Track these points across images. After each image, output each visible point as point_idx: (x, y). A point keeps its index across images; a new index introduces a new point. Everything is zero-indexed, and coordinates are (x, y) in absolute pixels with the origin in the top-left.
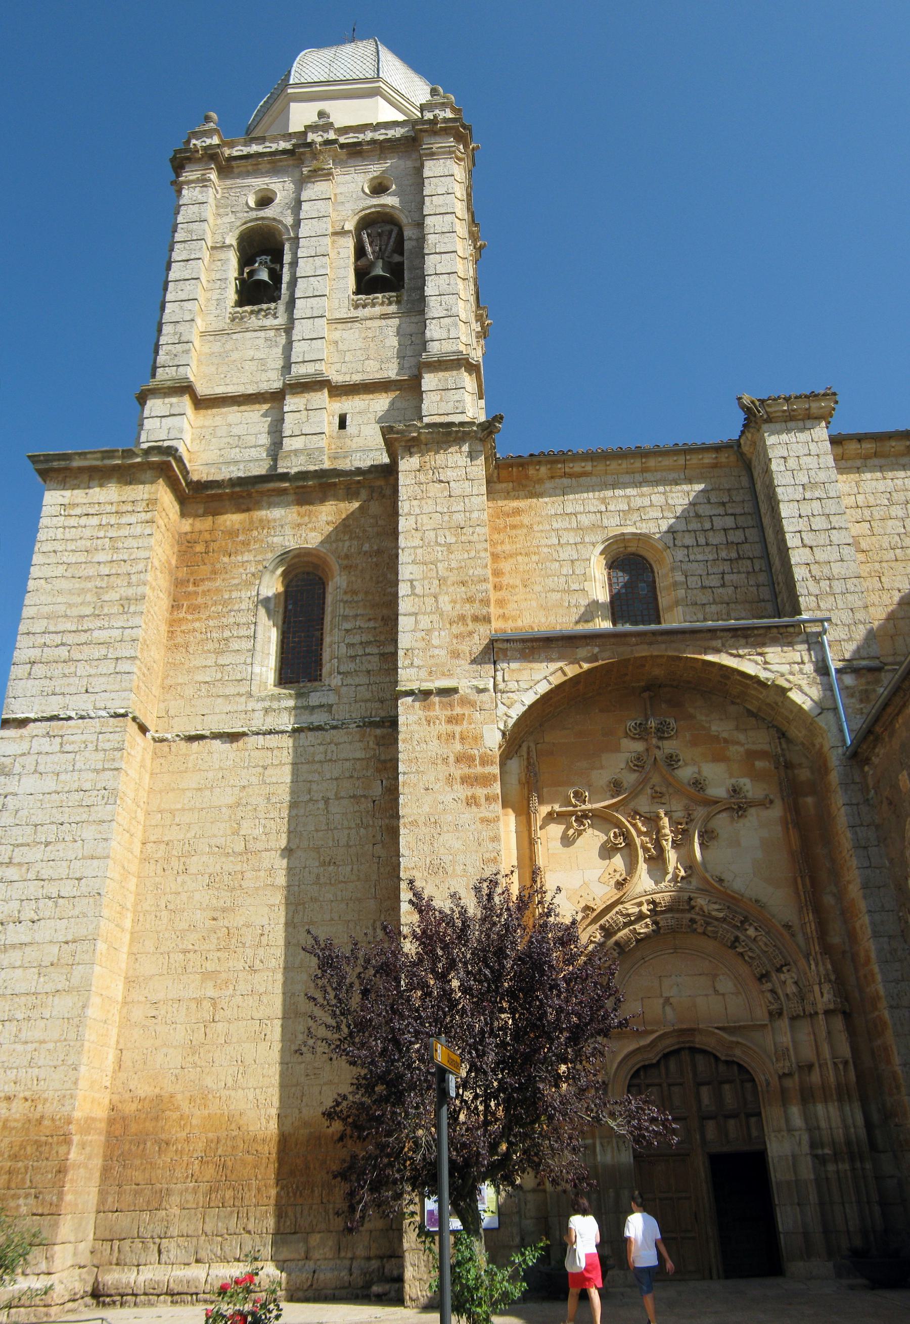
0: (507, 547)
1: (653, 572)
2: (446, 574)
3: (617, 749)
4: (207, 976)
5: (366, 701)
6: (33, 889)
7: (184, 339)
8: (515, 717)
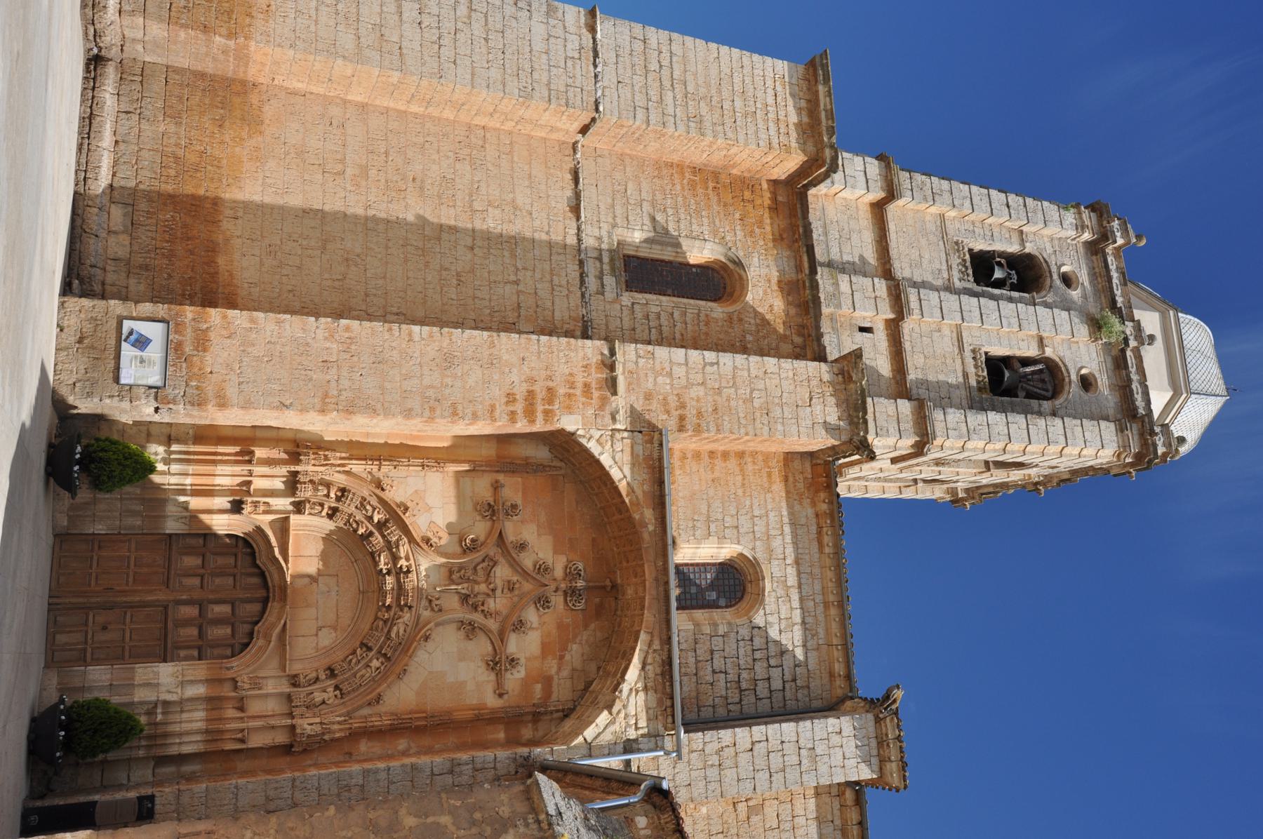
0: (750, 467)
1: (727, 607)
2: (724, 395)
3: (556, 552)
4: (364, 170)
5: (607, 325)
6: (448, 25)
7: (937, 197)
8: (589, 446)
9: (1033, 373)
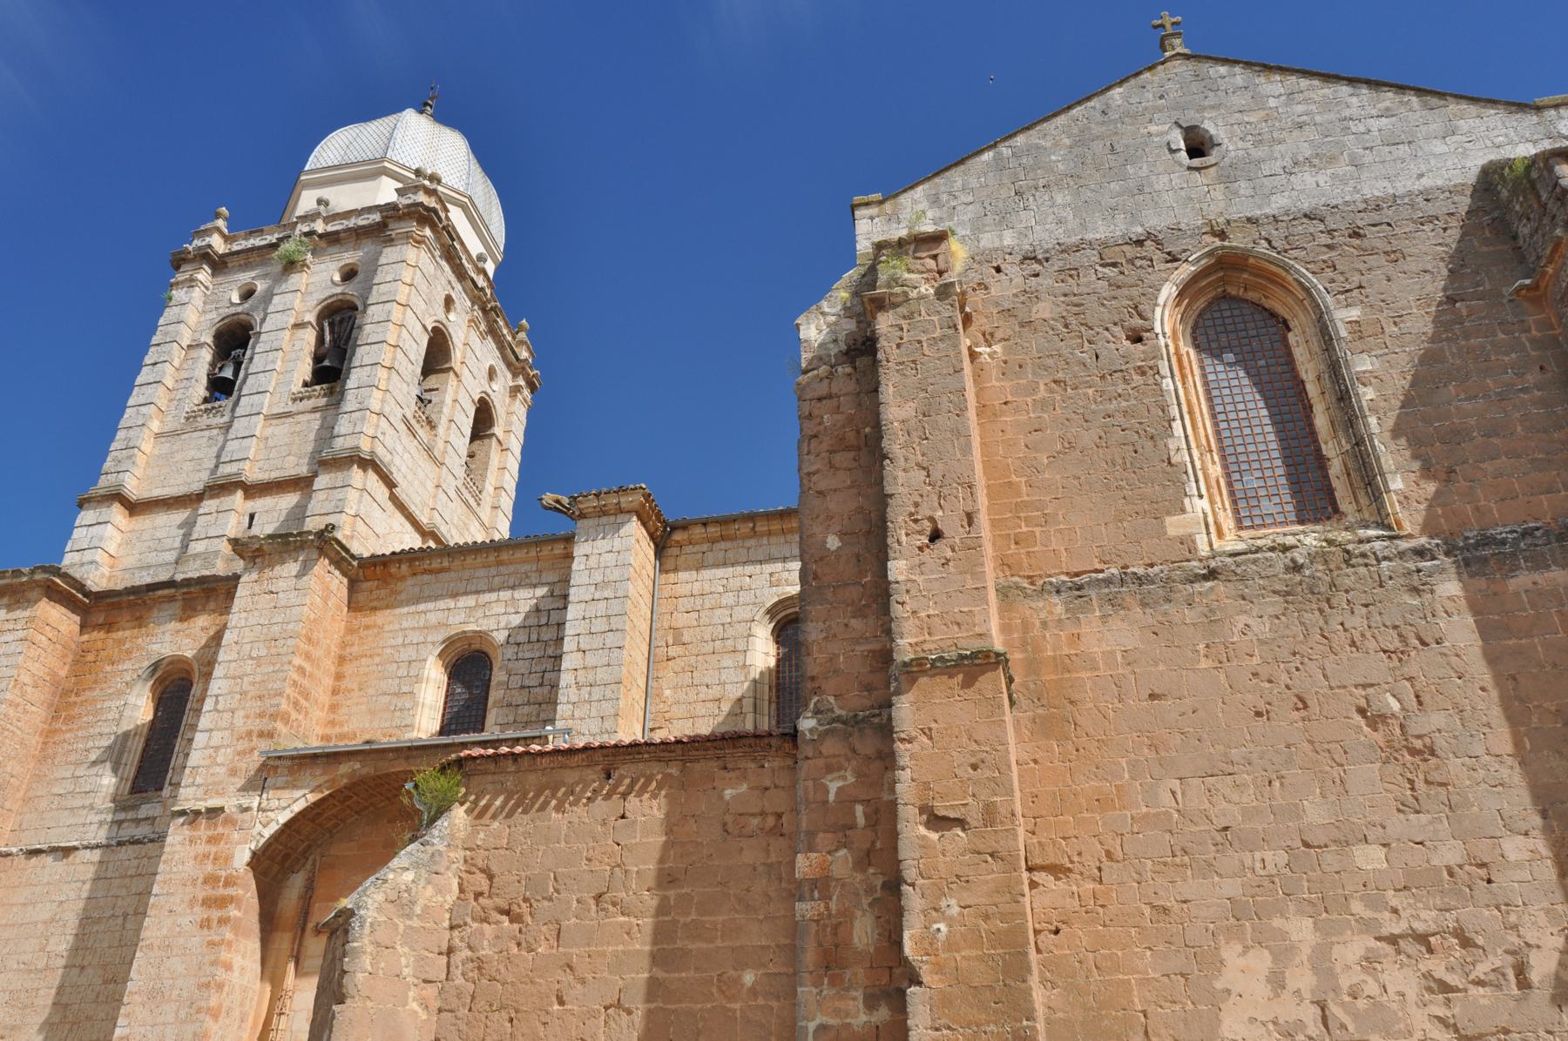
0: (355, 649)
9: (332, 332)
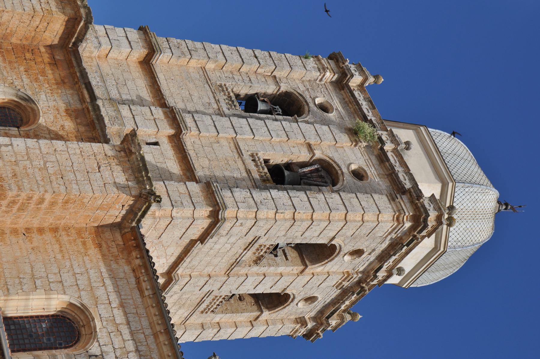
0: (65, 238)
7: (192, 52)
9: (311, 172)
